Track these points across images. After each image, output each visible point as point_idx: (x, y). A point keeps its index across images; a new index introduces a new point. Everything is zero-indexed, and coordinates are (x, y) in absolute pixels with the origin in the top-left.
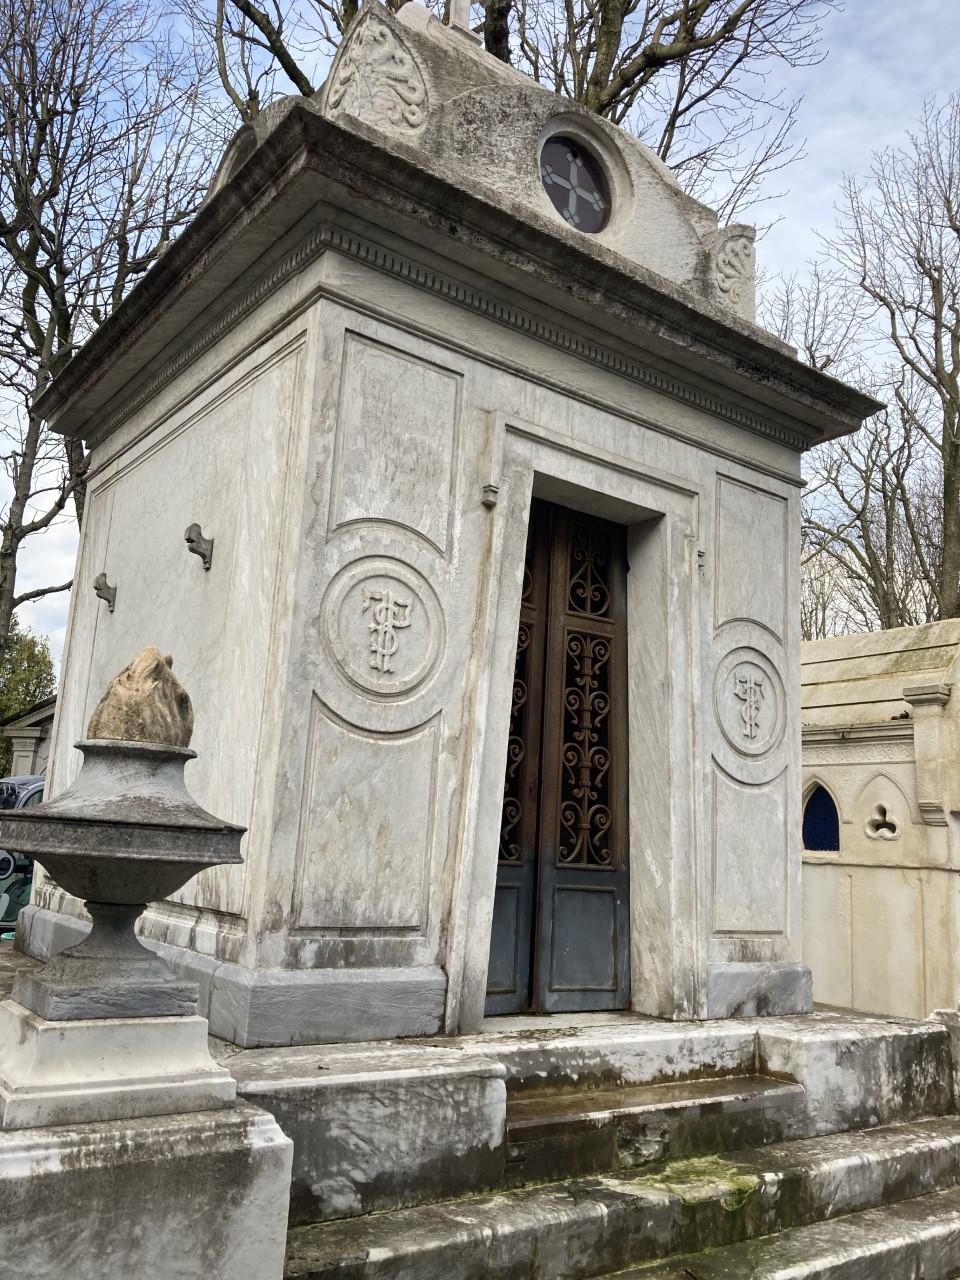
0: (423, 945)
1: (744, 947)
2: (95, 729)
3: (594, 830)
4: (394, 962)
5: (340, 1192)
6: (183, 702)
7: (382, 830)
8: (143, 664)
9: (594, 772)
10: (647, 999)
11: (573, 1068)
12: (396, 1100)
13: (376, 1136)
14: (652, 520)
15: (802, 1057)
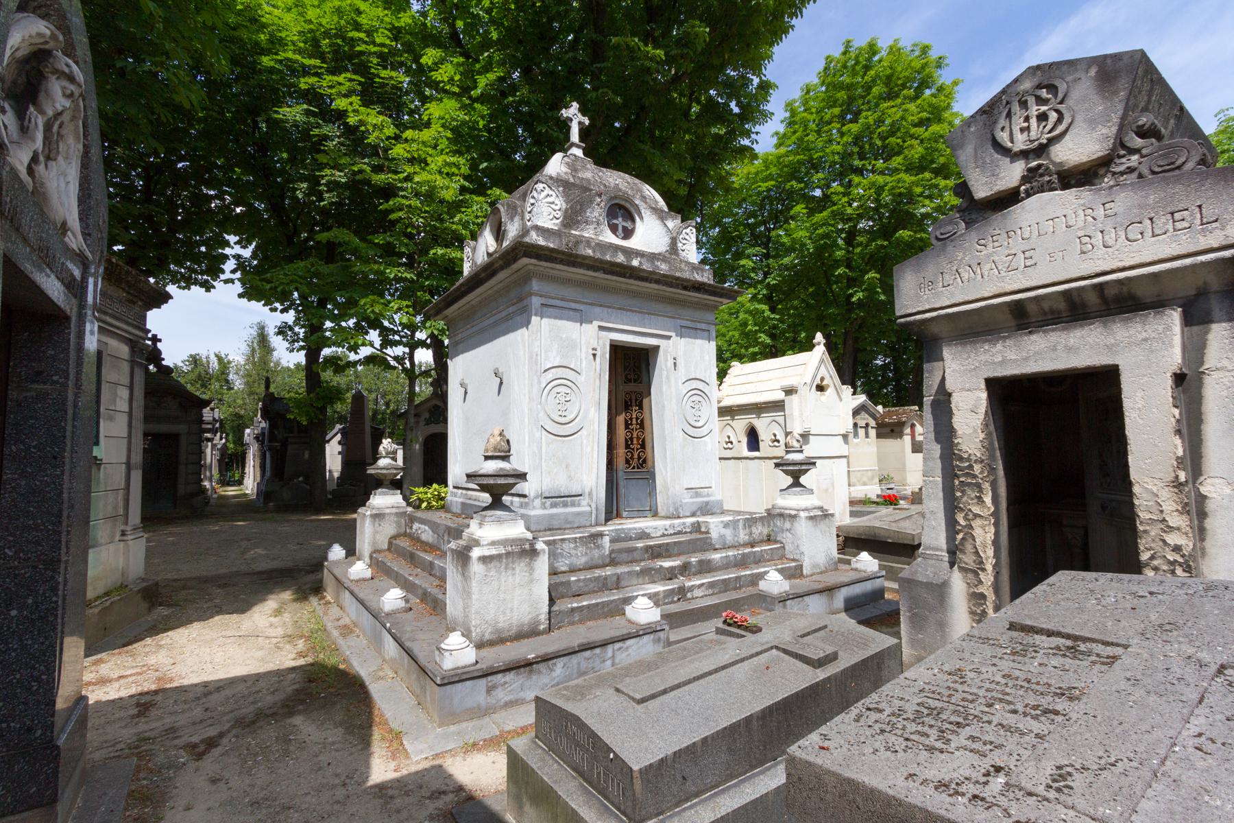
2: (486, 450)
3: (639, 458)
4: (573, 505)
6: (508, 441)
8: (497, 432)
9: (638, 438)
10: (661, 512)
14: (657, 348)
15: (712, 526)
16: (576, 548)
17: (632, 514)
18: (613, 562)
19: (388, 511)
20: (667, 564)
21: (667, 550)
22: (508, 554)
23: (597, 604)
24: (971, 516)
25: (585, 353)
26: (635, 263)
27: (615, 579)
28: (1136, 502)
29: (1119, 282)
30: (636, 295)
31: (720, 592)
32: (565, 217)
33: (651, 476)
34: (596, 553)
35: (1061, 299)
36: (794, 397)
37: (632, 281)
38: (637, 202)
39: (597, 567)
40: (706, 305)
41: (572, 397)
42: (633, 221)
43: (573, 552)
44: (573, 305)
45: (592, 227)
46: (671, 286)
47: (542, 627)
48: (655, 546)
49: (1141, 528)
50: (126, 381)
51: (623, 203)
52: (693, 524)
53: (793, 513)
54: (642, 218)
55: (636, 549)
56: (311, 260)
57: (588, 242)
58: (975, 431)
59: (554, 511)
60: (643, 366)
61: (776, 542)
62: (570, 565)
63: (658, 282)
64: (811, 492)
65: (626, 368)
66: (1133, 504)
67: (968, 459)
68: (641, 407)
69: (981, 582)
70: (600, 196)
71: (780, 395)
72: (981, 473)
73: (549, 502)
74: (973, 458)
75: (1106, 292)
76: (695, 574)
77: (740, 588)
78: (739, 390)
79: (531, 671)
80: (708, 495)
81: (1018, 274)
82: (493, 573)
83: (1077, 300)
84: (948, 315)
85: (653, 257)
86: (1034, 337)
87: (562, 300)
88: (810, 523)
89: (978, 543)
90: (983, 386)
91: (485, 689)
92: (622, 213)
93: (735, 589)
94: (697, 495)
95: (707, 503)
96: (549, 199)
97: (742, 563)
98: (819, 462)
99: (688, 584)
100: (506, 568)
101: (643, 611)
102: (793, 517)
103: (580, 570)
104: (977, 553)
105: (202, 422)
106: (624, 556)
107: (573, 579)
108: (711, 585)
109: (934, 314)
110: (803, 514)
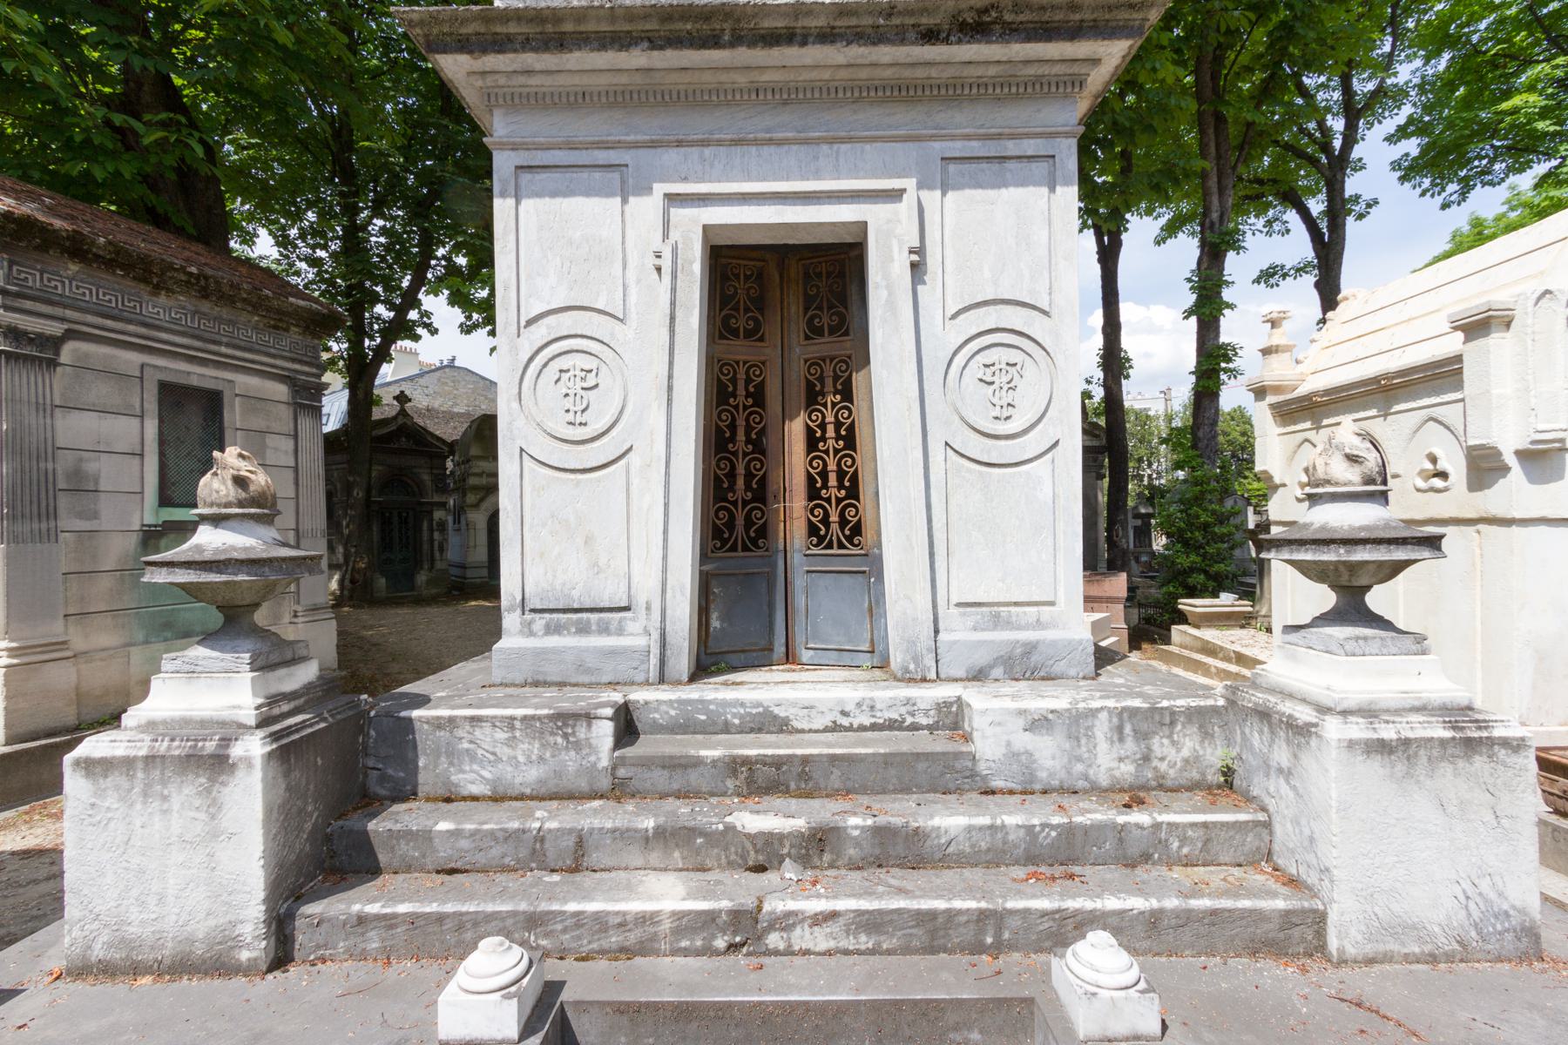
0: (633, 619)
1: (997, 616)
3: (749, 522)
4: (604, 630)
5: (473, 783)
7: (588, 540)
10: (897, 659)
11: (734, 715)
12: (512, 728)
13: (497, 750)
16: (511, 742)
18: (618, 790)
20: (755, 820)
21: (804, 776)
22: (150, 760)
23: (440, 918)
25: (639, 261)
27: (570, 842)
30: (787, 96)
31: (906, 950)
33: (871, 570)
34: (571, 760)
36: (1495, 342)
37: (743, 55)
40: (1038, 81)
43: (504, 752)
44: (602, 156)
47: (245, 955)
48: (763, 761)
52: (943, 706)
53: (1304, 714)
55: (698, 762)
59: (554, 641)
60: (853, 290)
62: (494, 784)
63: (827, 36)
65: (808, 302)
68: (847, 394)
71: (1454, 343)
73: (540, 621)
80: (1039, 624)
88: (1375, 767)
94: (997, 622)
95: (1030, 648)
98: (1453, 539)
99: (776, 905)
100: (145, 795)
102: (1301, 732)
106: (659, 778)
107: (443, 826)
108: (871, 922)
110: (1333, 729)
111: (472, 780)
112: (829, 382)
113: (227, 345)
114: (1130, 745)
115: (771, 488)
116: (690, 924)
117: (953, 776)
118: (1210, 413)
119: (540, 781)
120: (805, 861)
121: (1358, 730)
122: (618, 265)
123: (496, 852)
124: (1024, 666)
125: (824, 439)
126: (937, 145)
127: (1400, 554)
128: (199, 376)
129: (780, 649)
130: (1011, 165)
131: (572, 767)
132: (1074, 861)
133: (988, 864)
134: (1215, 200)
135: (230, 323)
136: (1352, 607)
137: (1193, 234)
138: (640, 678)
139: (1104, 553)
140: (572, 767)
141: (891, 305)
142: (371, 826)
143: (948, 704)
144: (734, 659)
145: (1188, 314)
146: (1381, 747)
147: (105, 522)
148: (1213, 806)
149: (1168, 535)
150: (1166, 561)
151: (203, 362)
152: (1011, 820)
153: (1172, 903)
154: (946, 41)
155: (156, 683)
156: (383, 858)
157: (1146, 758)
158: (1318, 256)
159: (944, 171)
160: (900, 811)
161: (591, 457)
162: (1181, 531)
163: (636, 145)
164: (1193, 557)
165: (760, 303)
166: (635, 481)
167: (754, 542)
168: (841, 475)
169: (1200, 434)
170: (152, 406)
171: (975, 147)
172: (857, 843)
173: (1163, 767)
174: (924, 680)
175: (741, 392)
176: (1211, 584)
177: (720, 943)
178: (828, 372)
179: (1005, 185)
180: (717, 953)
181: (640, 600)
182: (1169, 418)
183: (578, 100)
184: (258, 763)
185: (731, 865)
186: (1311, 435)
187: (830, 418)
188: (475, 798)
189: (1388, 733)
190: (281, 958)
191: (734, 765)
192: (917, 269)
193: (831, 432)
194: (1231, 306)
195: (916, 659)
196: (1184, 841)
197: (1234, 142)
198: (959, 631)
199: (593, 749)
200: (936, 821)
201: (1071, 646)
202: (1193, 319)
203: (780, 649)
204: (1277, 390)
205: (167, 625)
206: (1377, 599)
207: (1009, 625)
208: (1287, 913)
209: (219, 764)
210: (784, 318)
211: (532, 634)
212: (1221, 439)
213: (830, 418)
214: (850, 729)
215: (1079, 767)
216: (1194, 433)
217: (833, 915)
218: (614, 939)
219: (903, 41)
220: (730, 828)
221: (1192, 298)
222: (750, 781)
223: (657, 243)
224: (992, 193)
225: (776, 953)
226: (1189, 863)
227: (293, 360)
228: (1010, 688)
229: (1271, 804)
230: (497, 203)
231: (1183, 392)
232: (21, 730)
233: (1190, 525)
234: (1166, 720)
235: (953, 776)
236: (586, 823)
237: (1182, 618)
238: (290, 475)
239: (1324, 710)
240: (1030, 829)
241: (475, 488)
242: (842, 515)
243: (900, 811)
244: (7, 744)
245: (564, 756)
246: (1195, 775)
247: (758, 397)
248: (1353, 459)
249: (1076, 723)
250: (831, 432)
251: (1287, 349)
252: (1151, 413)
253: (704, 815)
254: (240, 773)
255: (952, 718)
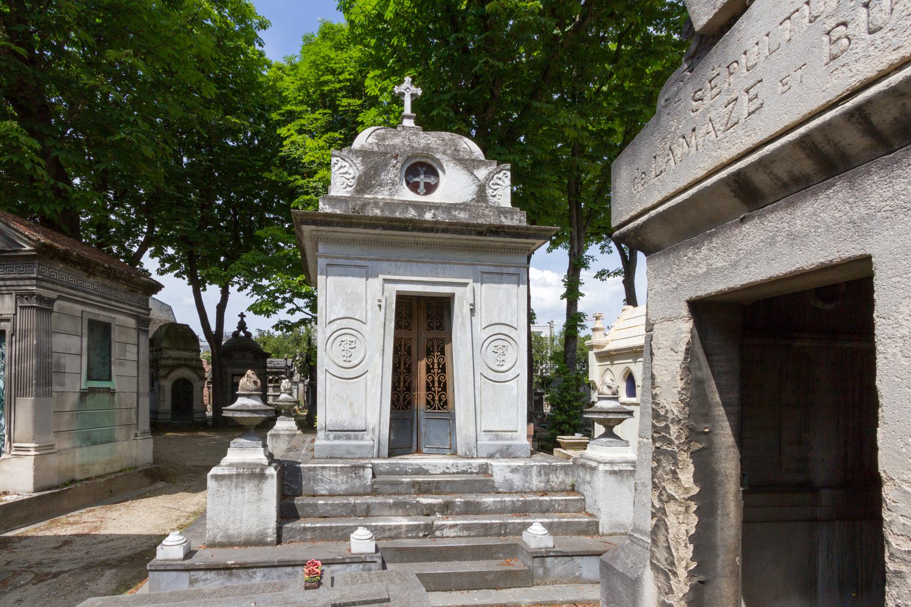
3: (405, 399)
4: (356, 438)
12: (336, 471)
15: (495, 469)
16: (336, 476)
17: (432, 451)
18: (374, 492)
19: (283, 432)
20: (425, 500)
21: (437, 488)
22: (238, 475)
23: (331, 528)
24: (664, 498)
25: (372, 303)
26: (428, 216)
27: (365, 507)
28: (886, 515)
29: (893, 92)
32: (358, 184)
34: (357, 482)
35: (800, 154)
37: (415, 233)
38: (438, 156)
39: (357, 495)
41: (358, 345)
42: (436, 175)
43: (333, 479)
45: (387, 188)
46: (463, 233)
47: (269, 539)
48: (424, 482)
49: (891, 566)
50: (135, 341)
51: (424, 160)
52: (481, 466)
53: (594, 464)
54: (444, 171)
55: (402, 483)
56: (252, 252)
57: (376, 203)
58: (674, 378)
59: (337, 442)
60: (446, 313)
61: (579, 493)
62: (330, 490)
63: (445, 231)
64: (627, 443)
65: (428, 317)
66: (881, 519)
67: (665, 418)
68: (443, 352)
69: (671, 590)
70: (396, 157)
72: (678, 437)
73: (332, 435)
74: (670, 416)
75: (875, 119)
76: (458, 514)
77: (505, 535)
78: (624, 333)
79: (231, 575)
80: (512, 439)
81: (739, 130)
82: (224, 489)
83: (828, 149)
84: (659, 215)
85: (464, 207)
86: (747, 227)
87: (347, 258)
88: (612, 479)
89: (671, 536)
90: (685, 311)
91: (187, 581)
92: (421, 171)
93: (499, 535)
94: (497, 438)
95: (509, 447)
96: (343, 170)
97: (516, 510)
100: (236, 486)
101: (361, 541)
102: (593, 469)
103: (340, 495)
104: (668, 548)
105: (267, 367)
106: (388, 488)
107: (321, 502)
108: (467, 527)
109: (645, 218)
110: (602, 467)
111: (322, 489)
112: (436, 347)
113: (115, 301)
114: (543, 477)
115: (413, 386)
116: (411, 529)
117: (488, 487)
118: (572, 346)
119: (346, 490)
120: (442, 513)
121: (608, 467)
122: (364, 303)
123: (339, 510)
124: (506, 453)
125: (433, 368)
126: (480, 267)
127: (621, 416)
128: (103, 316)
129: (415, 448)
130: (504, 276)
131: (357, 484)
132: (526, 512)
133: (500, 513)
134: (576, 244)
135: (116, 289)
136: (609, 433)
137: (566, 247)
138: (370, 456)
139: (534, 413)
140: (357, 484)
141: (463, 323)
142: (295, 502)
143: (483, 465)
144: (399, 451)
145: (563, 297)
146: (614, 473)
147: (67, 388)
148: (568, 495)
149: (552, 406)
150: (551, 418)
151: (104, 309)
152: (507, 499)
153: (556, 520)
154: (485, 235)
155: (229, 451)
156: (300, 513)
157: (548, 482)
158: (624, 267)
159: (482, 276)
160: (471, 498)
161: (352, 374)
162: (558, 404)
163: (372, 260)
164: (564, 417)
165: (410, 316)
166: (369, 383)
167: (442, 407)
168: (440, 382)
169: (568, 356)
170: (85, 331)
171: (492, 269)
172: (459, 507)
173: (553, 484)
174: (472, 458)
175: (403, 350)
176: (572, 429)
177: (421, 535)
178: (435, 344)
179: (503, 283)
180: (420, 538)
181: (371, 427)
182: (552, 340)
183: (352, 242)
184: (275, 476)
185: (418, 514)
186: (610, 367)
187: (436, 361)
188: (323, 495)
189: (616, 468)
190: (279, 541)
191: (414, 484)
192: (472, 311)
193: (436, 366)
194: (582, 295)
195: (470, 450)
196: (559, 505)
197: (585, 215)
198: (484, 441)
199: (365, 478)
200: (484, 500)
201: (523, 446)
202: (565, 300)
203: (415, 448)
204: (598, 347)
205: (88, 439)
206: (617, 430)
207: (502, 439)
208: (588, 522)
209: (262, 477)
210: (423, 326)
211: (329, 439)
212: (579, 352)
213: (436, 361)
214: (449, 473)
215: (527, 485)
216: (565, 356)
217: (456, 525)
218: (387, 534)
219: (471, 234)
220: (418, 502)
221: (564, 290)
222: (419, 489)
223: (379, 296)
224: (498, 285)
225: (438, 537)
226: (561, 512)
227: (139, 307)
228: (502, 460)
229: (585, 493)
230: (319, 277)
231: (561, 322)
232: (43, 483)
233: (562, 401)
234: (553, 469)
235: (488, 487)
236: (370, 501)
237: (558, 445)
238: (135, 364)
239: (599, 462)
240: (513, 502)
241: (165, 366)
242: (440, 397)
243: (471, 498)
244: (34, 492)
245: (355, 481)
246: (563, 487)
247: (409, 352)
248: (609, 387)
249: (527, 470)
250: (436, 366)
251: (602, 329)
252: (543, 335)
253: (407, 498)
254: (269, 480)
255: (484, 470)
